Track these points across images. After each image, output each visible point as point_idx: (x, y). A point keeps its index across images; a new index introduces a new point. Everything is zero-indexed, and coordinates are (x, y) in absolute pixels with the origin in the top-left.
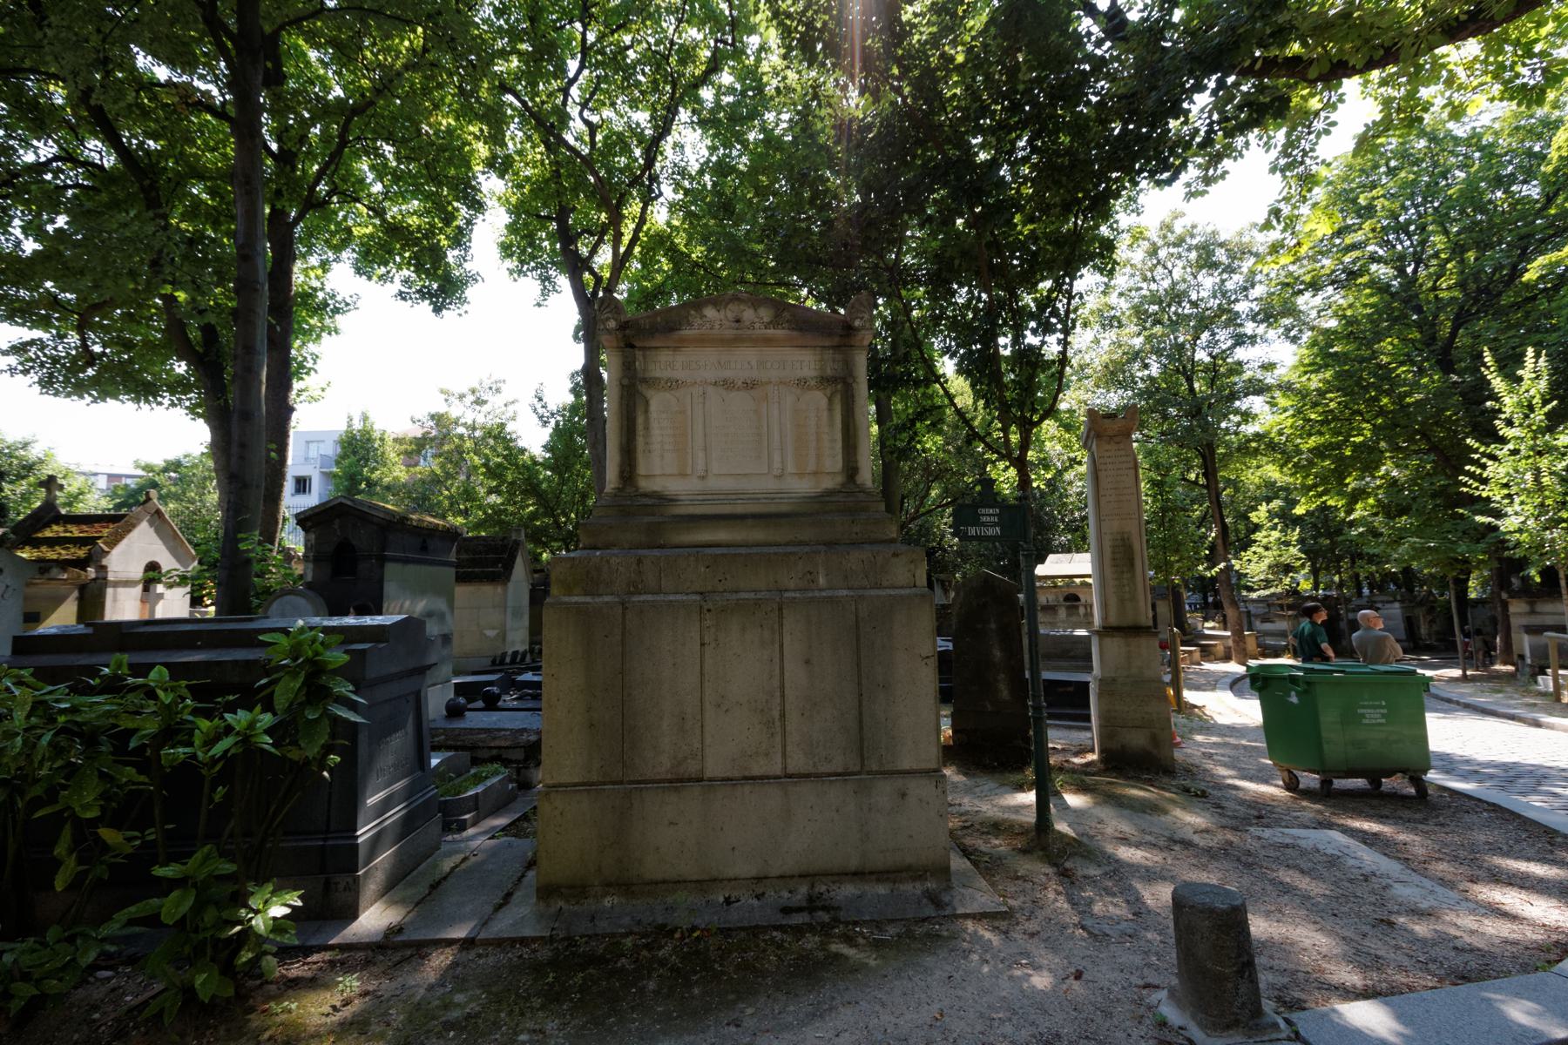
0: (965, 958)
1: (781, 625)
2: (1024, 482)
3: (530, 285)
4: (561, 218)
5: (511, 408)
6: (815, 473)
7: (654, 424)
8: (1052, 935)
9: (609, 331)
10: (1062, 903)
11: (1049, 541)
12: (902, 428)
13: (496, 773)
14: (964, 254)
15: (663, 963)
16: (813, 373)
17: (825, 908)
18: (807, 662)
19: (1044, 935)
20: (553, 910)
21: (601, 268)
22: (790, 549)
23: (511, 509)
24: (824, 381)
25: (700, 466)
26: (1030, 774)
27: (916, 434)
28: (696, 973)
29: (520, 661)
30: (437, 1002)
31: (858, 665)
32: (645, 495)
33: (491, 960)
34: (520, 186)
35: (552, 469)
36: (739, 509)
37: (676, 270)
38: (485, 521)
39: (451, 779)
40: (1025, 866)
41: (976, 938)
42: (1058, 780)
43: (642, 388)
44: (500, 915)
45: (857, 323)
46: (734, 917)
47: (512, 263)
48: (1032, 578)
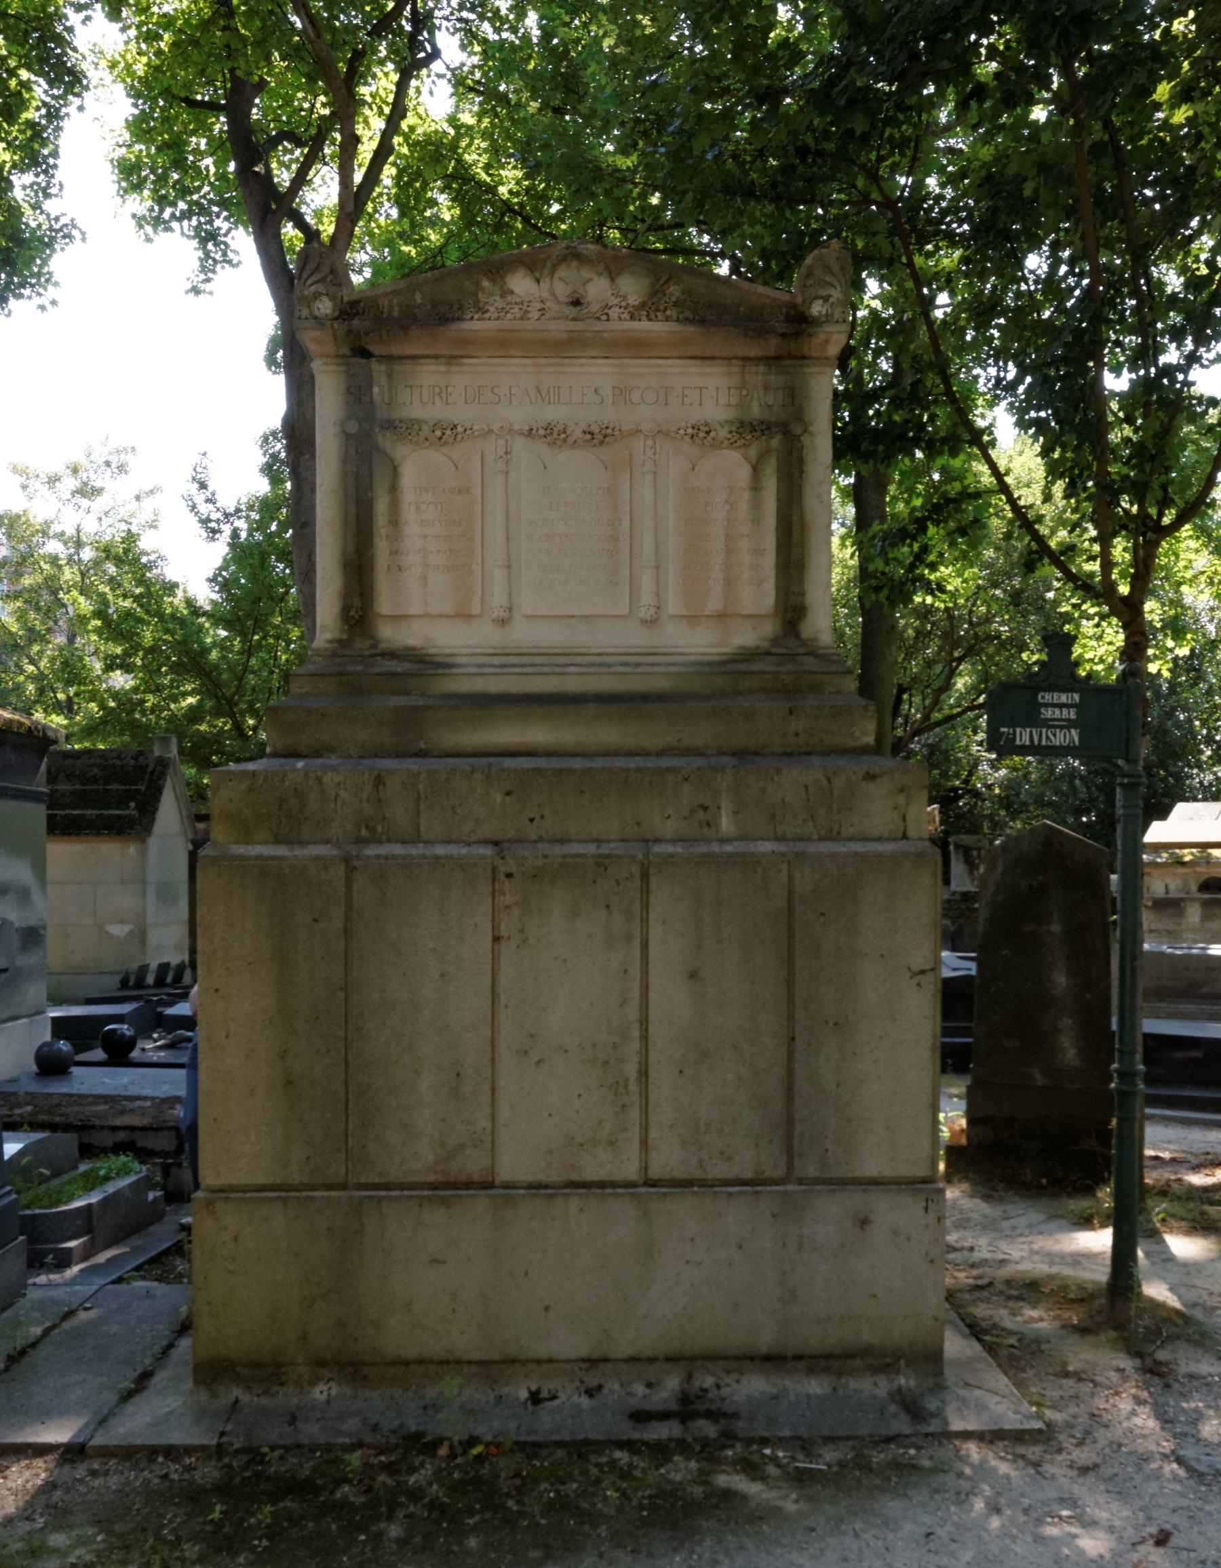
0: (959, 1503)
1: (646, 906)
2: (1134, 651)
3: (178, 248)
4: (236, 107)
5: (148, 504)
6: (722, 616)
7: (409, 515)
8: (1116, 1470)
9: (319, 321)
10: (1145, 1421)
11: (1179, 778)
12: (902, 535)
13: (124, 1171)
14: (1043, 167)
15: (415, 1495)
16: (729, 414)
17: (710, 1415)
18: (693, 975)
19: (1107, 1471)
20: (225, 1401)
21: (318, 214)
22: (664, 763)
23: (151, 700)
24: (747, 429)
25: (498, 599)
26: (1105, 1196)
27: (925, 549)
28: (472, 1512)
29: (173, 980)
30: (19, 1545)
32: (392, 655)
33: (114, 1482)
34: (151, 37)
35: (228, 625)
36: (572, 684)
37: (468, 219)
38: (104, 721)
39: (45, 1180)
40: (1079, 1355)
41: (983, 1470)
42: (1159, 1209)
43: (385, 440)
44: (129, 1408)
45: (817, 309)
46: (546, 1424)
47: (140, 203)
48: (1135, 845)
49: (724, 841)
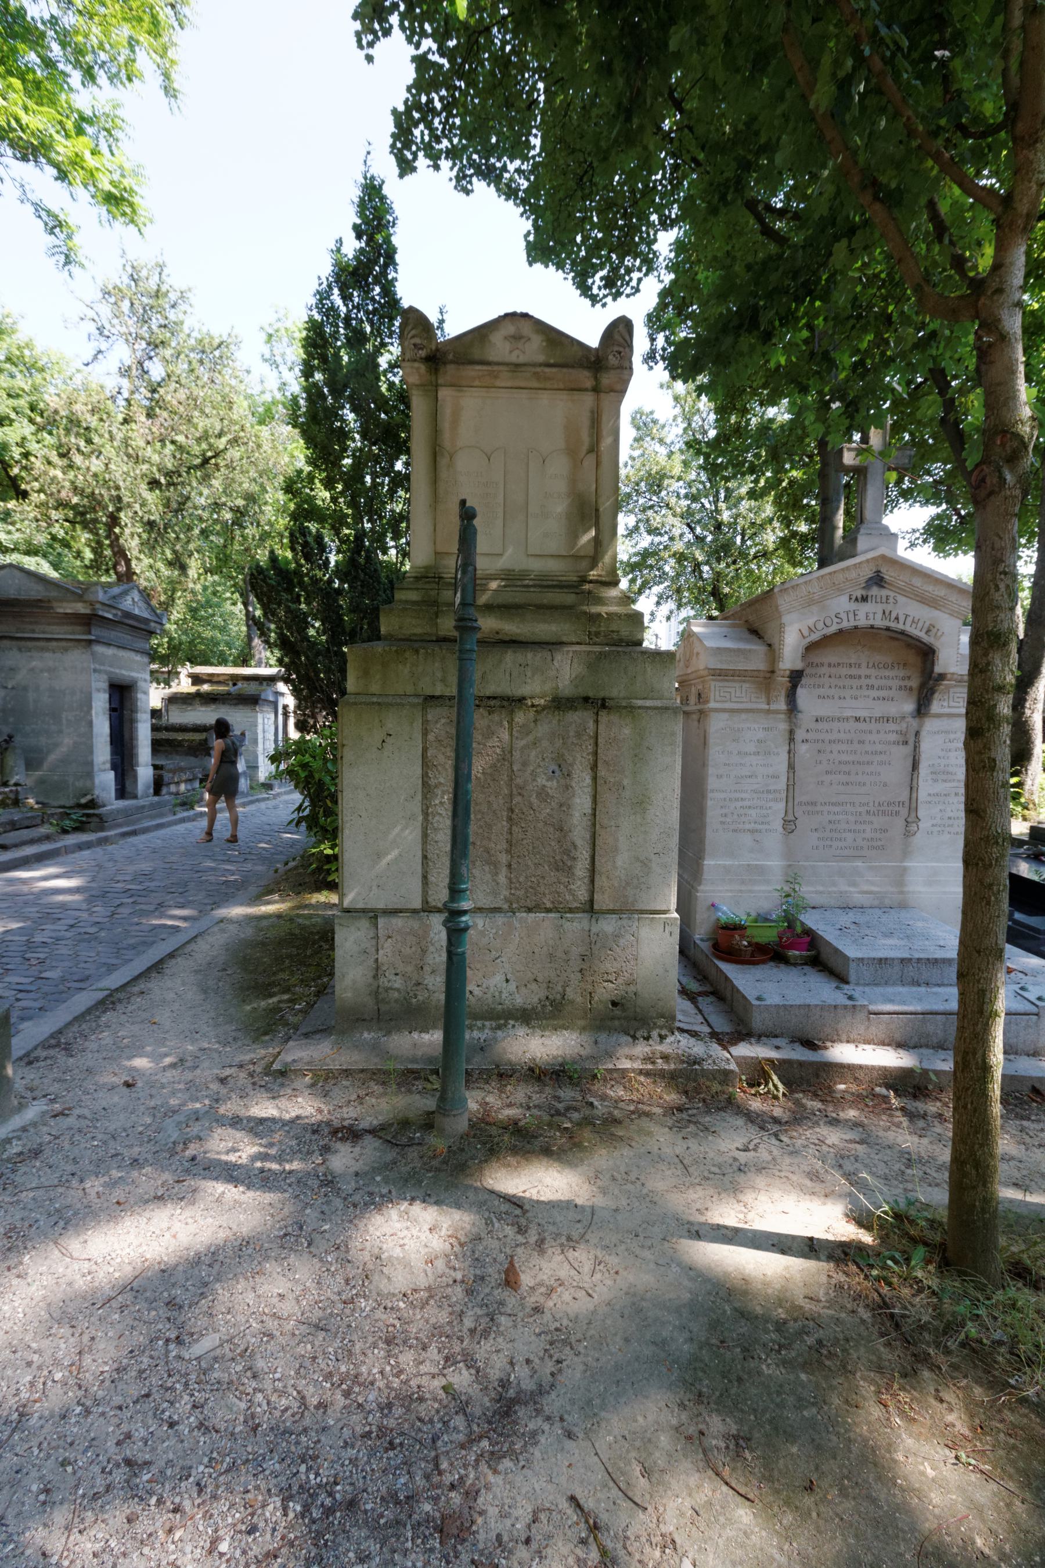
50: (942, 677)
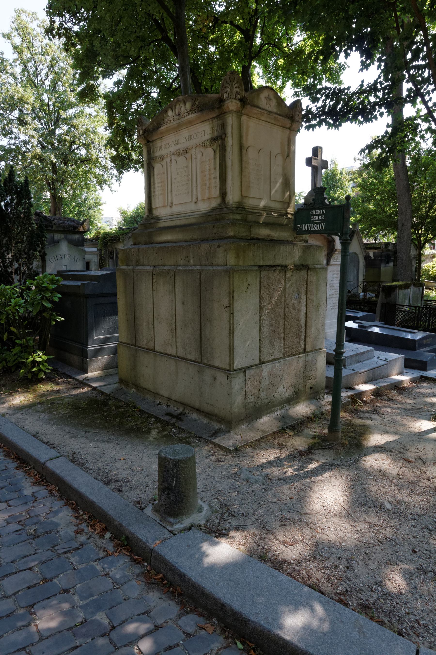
6: (209, 198)
18: (183, 303)
31: (200, 307)
49: (191, 266)
50: (336, 250)
